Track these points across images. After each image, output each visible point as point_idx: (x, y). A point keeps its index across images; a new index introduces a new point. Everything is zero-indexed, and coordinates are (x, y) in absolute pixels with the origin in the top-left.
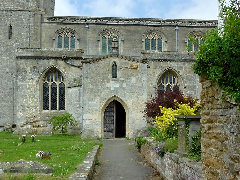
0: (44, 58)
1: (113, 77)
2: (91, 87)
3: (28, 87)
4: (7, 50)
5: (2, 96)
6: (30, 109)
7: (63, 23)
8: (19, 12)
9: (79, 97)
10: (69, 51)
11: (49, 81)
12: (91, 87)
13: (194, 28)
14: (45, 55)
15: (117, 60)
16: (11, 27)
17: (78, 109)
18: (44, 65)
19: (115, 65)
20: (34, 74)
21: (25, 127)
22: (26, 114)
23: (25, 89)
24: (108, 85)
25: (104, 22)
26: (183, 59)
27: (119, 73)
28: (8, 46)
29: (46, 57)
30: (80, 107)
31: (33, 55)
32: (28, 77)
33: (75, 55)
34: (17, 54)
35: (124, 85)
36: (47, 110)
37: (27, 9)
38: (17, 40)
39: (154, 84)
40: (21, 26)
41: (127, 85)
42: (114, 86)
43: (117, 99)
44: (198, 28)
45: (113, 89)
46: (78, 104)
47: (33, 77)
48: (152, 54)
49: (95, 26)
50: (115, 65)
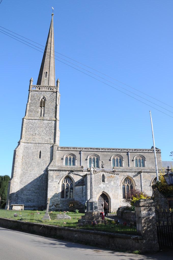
1: (102, 182)
3: (54, 186)
4: (38, 164)
7: (69, 151)
9: (82, 191)
10: (76, 167)
11: (65, 183)
14: (64, 169)
15: (104, 173)
16: (40, 152)
17: (82, 198)
23: (52, 187)
24: (100, 186)
26: (135, 171)
27: (106, 180)
28: (38, 162)
30: (83, 197)
32: (54, 180)
33: (79, 169)
35: (108, 186)
36: (104, 194)
37: (49, 143)
40: (46, 152)
41: (109, 186)
42: (103, 186)
43: (104, 193)
45: (102, 188)
46: (81, 195)
49: (85, 152)
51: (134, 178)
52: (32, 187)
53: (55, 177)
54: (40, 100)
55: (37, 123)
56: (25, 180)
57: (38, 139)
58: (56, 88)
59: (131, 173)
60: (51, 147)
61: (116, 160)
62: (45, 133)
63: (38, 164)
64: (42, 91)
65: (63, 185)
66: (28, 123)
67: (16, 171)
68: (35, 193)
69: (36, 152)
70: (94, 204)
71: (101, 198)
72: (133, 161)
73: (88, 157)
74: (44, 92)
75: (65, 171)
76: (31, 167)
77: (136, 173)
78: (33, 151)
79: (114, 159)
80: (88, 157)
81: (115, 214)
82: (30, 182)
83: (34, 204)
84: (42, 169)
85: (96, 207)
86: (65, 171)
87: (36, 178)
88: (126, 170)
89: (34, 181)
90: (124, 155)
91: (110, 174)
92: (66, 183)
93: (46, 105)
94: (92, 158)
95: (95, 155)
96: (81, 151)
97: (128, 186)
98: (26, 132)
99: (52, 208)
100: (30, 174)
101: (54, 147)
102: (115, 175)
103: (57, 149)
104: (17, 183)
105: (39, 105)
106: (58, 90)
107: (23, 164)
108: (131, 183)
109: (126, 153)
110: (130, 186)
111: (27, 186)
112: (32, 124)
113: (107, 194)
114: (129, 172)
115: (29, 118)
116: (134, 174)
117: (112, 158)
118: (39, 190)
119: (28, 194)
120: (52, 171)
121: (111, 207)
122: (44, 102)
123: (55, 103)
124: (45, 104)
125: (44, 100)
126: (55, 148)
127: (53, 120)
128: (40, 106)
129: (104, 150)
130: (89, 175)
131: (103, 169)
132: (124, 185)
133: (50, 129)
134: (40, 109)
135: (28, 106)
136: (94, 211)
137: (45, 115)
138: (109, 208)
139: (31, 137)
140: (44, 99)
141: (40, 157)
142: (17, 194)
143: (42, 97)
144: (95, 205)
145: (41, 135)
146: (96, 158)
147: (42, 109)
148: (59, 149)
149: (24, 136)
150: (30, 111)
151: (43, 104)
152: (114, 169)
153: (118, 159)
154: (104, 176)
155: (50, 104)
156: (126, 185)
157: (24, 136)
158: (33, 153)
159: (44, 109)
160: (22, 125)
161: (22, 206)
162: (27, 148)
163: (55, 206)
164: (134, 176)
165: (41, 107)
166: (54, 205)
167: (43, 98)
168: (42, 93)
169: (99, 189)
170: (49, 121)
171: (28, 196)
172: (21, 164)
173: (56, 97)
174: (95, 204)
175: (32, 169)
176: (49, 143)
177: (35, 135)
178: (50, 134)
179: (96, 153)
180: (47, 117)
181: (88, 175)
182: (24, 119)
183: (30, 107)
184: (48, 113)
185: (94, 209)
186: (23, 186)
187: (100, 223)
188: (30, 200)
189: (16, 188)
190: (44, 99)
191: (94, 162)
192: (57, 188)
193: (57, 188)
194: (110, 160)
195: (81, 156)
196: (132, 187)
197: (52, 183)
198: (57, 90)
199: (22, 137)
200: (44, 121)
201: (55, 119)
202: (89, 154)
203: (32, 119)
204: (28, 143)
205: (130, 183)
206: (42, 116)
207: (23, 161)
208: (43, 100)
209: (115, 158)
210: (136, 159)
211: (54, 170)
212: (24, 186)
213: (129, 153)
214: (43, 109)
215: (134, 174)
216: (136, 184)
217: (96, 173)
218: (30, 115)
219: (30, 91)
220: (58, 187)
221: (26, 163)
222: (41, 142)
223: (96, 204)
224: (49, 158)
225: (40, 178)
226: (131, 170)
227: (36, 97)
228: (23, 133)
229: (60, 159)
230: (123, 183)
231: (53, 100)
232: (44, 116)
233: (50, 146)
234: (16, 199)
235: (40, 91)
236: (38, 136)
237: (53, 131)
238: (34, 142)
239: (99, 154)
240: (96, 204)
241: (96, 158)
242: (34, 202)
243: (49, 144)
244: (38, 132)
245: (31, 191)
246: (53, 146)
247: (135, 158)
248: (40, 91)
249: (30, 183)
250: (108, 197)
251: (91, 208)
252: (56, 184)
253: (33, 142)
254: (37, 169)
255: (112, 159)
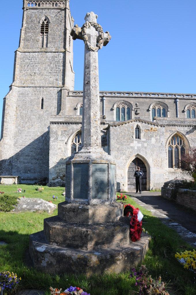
0: (72, 123)
1: (136, 138)
2: (118, 146)
3: (59, 147)
4: (39, 118)
5: (34, 155)
6: (61, 165)
8: (50, 88)
11: (76, 143)
12: (118, 146)
13: (191, 101)
14: (74, 120)
15: (140, 124)
16: (43, 100)
18: (73, 129)
19: (138, 128)
20: (64, 136)
21: (56, 181)
22: (57, 170)
24: (132, 145)
25: (127, 95)
26: (188, 124)
27: (142, 135)
29: (75, 122)
31: (64, 121)
34: (51, 121)
35: (146, 145)
37: (56, 86)
38: (47, 110)
39: (5, 193)
40: (50, 99)
41: (148, 145)
44: (194, 101)
45: (136, 148)
47: (63, 139)
48: (163, 120)
49: (110, 98)
50: (138, 128)
51: (187, 136)
52: (31, 151)
53: (60, 133)
54: (41, 23)
55: (37, 57)
56: (21, 141)
57: (38, 81)
58: (65, 3)
59: (182, 127)
60: (58, 92)
61: (157, 110)
62: (50, 71)
63: (40, 117)
64: (42, 9)
65: (74, 145)
66: (24, 57)
67: (6, 129)
68: (35, 159)
69: (36, 101)
70: (92, 168)
71: (134, 165)
72: (183, 112)
73: (115, 106)
74: (46, 10)
75: (76, 124)
76: (29, 122)
77: (192, 128)
78: (32, 98)
79: (154, 109)
80: (115, 106)
81: (159, 194)
82: (29, 143)
83: (36, 175)
84: (45, 125)
85: (102, 182)
86: (76, 123)
87: (36, 138)
88: (174, 123)
89: (34, 142)
90: (170, 103)
91: (150, 125)
92: (78, 142)
93: (49, 30)
94: (121, 107)
95: (125, 103)
96: (103, 96)
97: (177, 147)
98: (21, 71)
99: (56, 181)
100: (28, 132)
101: (62, 92)
102: (157, 128)
103: (67, 94)
104: (10, 146)
105: (39, 30)
106: (68, 6)
107: (18, 118)
108: (182, 144)
109: (173, 100)
110: (180, 148)
111: (24, 149)
112: (30, 59)
113: (143, 158)
114: (179, 126)
115: (25, 51)
116: (187, 129)
117: (151, 107)
118: (41, 155)
119: (26, 161)
120: (56, 124)
121: (150, 180)
122: (47, 26)
123: (64, 26)
124: (48, 28)
125: (47, 23)
126: (64, 93)
127: (62, 52)
128: (41, 32)
129: (139, 96)
130: (112, 126)
131: (138, 116)
132: (171, 147)
133: (56, 66)
134: (41, 37)
135: (23, 32)
136: (94, 201)
137: (49, 45)
138: (148, 183)
139: (29, 78)
140: (46, 21)
141: (42, 108)
142: (10, 162)
143: (43, 18)
144: (98, 175)
145: (42, 75)
146: (126, 107)
147: (43, 36)
148: (71, 94)
149: (18, 77)
150: (26, 40)
151: (45, 31)
152: (155, 121)
153: (160, 110)
154: (138, 128)
155: (55, 27)
156: (174, 146)
157: (18, 77)
158: (31, 101)
159: (47, 36)
160: (15, 61)
161: (14, 178)
162: (22, 94)
163: (61, 178)
164: (188, 133)
165: (43, 34)
166: (59, 177)
167: (45, 20)
168: (44, 12)
169: (131, 150)
170: (55, 53)
171: (26, 165)
172: (15, 119)
173: (65, 16)
174: (96, 170)
175: (31, 124)
176: (55, 85)
177: (34, 75)
178: (56, 72)
179: (126, 99)
180: (51, 47)
181: (111, 127)
182: (17, 52)
183: (25, 33)
184: (53, 42)
185: (92, 193)
186: (18, 150)
187: (116, 269)
188: (29, 170)
189: (9, 153)
190: (46, 21)
191: (124, 113)
192: (63, 150)
193: (63, 150)
194: (148, 110)
195: (103, 104)
196: (183, 149)
197: (56, 143)
198: (66, 6)
199: (15, 78)
200: (47, 53)
201: (63, 50)
202: (116, 102)
203: (30, 51)
204: (24, 87)
205: (181, 144)
206: (45, 46)
207: (18, 114)
208: (45, 22)
209: (157, 108)
210: (189, 110)
211: (58, 123)
212: (20, 149)
213: (178, 100)
214: (45, 37)
215: (187, 129)
216: (190, 145)
217: (126, 124)
218: (26, 46)
219: (25, 9)
220: (66, 149)
221: (22, 117)
222: (43, 85)
223: (102, 170)
224: (55, 108)
225: (43, 138)
226: (182, 122)
227: (34, 19)
228: (16, 73)
229: (72, 109)
230: (169, 144)
231: (61, 21)
232: (47, 46)
233: (56, 90)
234: (9, 169)
235: (40, 9)
236: (39, 77)
237: (62, 68)
238: (33, 85)
239: (132, 101)
240: (102, 170)
241: (126, 107)
242: (35, 173)
243: (55, 87)
244: (38, 70)
245: (30, 157)
246: (61, 90)
247: (186, 109)
248: (40, 9)
249: (29, 145)
250: (146, 165)
251: (79, 188)
252: (62, 145)
253: (31, 85)
254: (38, 125)
255: (151, 109)
